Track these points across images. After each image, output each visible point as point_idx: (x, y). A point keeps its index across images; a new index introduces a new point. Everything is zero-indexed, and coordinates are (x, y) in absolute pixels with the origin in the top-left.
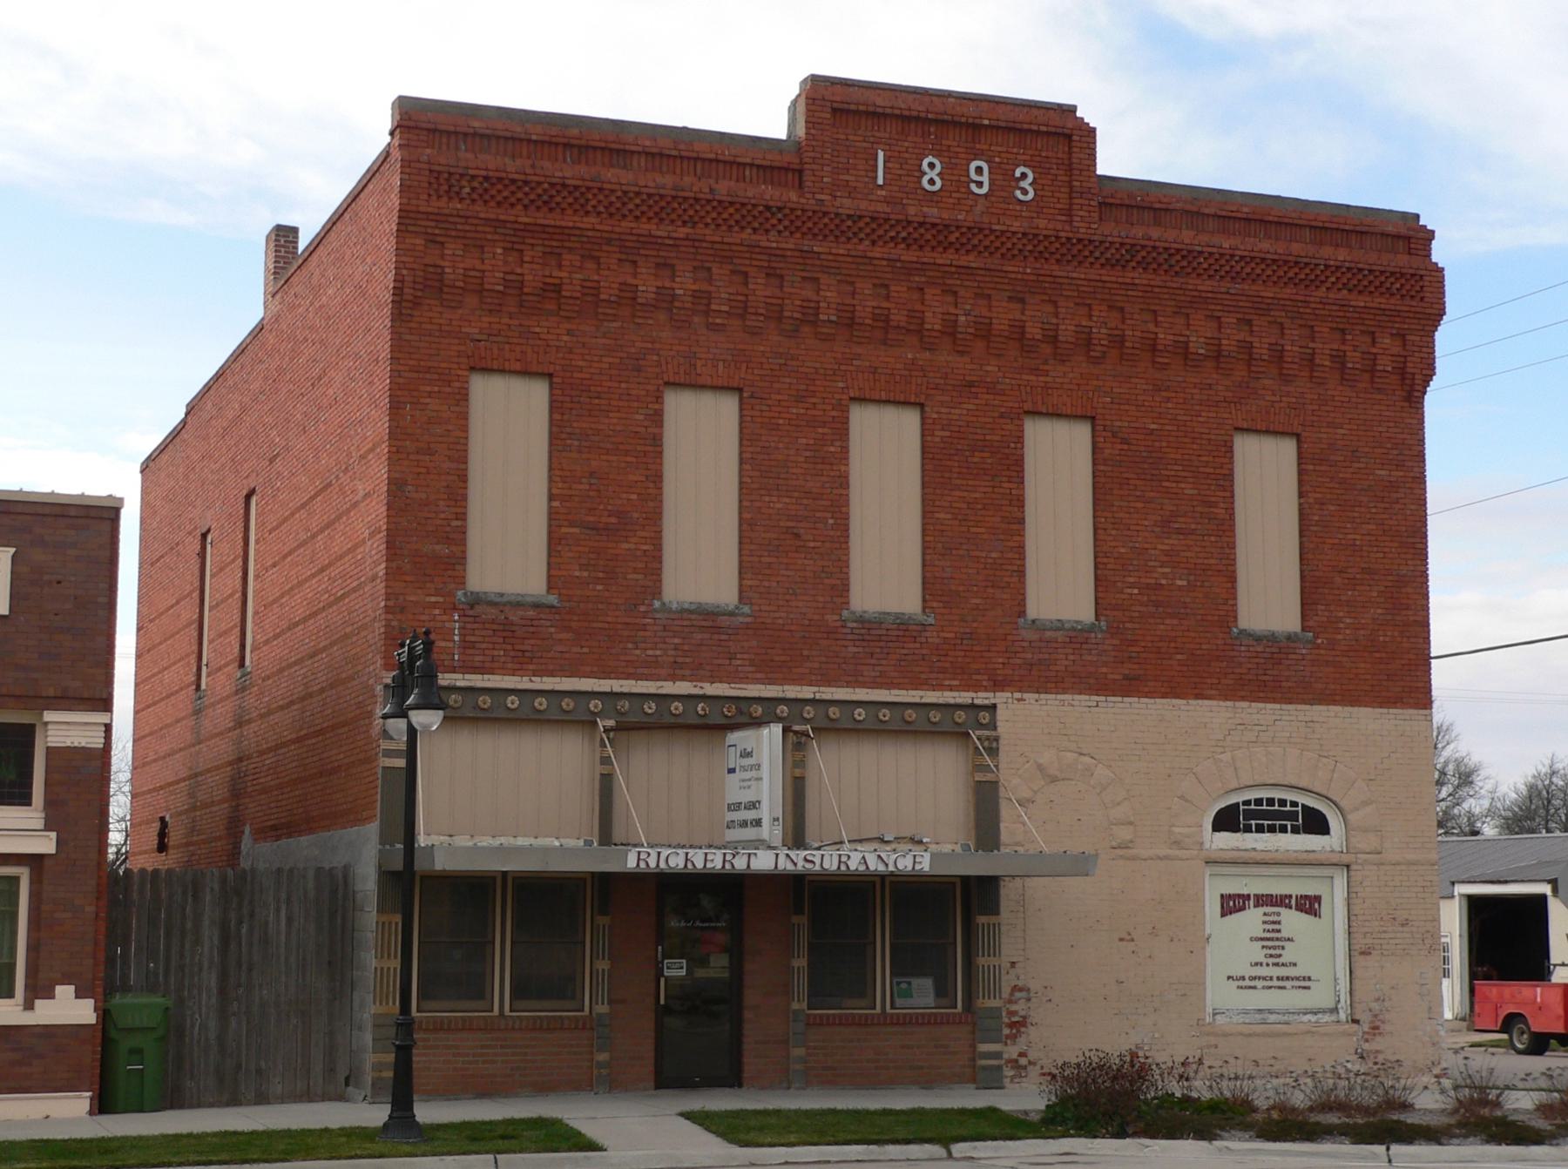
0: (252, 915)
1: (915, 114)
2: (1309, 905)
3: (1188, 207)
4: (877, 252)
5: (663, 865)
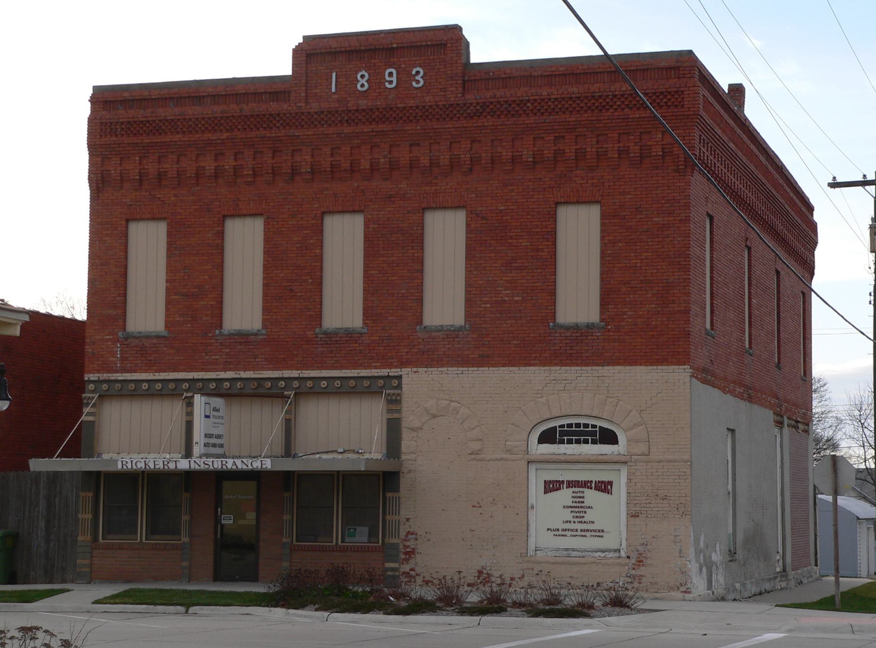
2: (605, 487)
5: (134, 467)
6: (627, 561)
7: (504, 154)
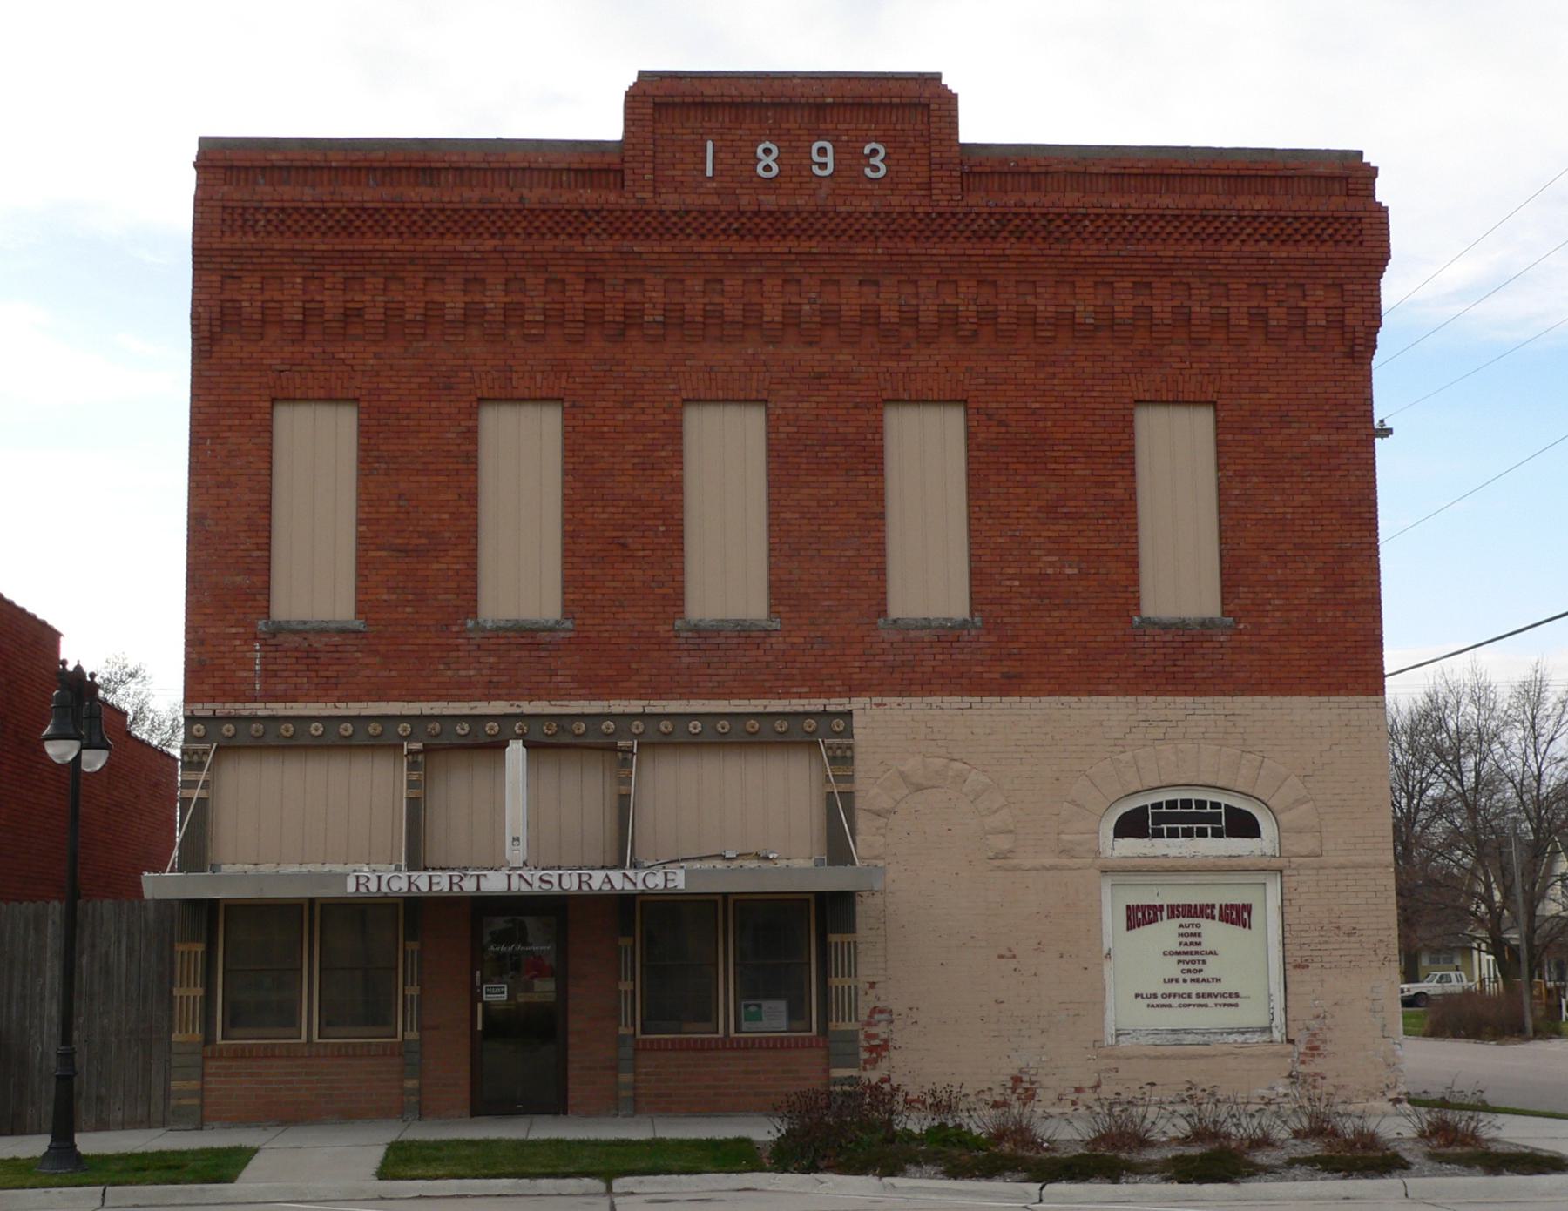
0: (93, 946)
1: (748, 100)
2: (1237, 915)
3: (1074, 168)
4: (705, 246)
5: (384, 889)
6: (1290, 1047)
7: (1041, 308)
